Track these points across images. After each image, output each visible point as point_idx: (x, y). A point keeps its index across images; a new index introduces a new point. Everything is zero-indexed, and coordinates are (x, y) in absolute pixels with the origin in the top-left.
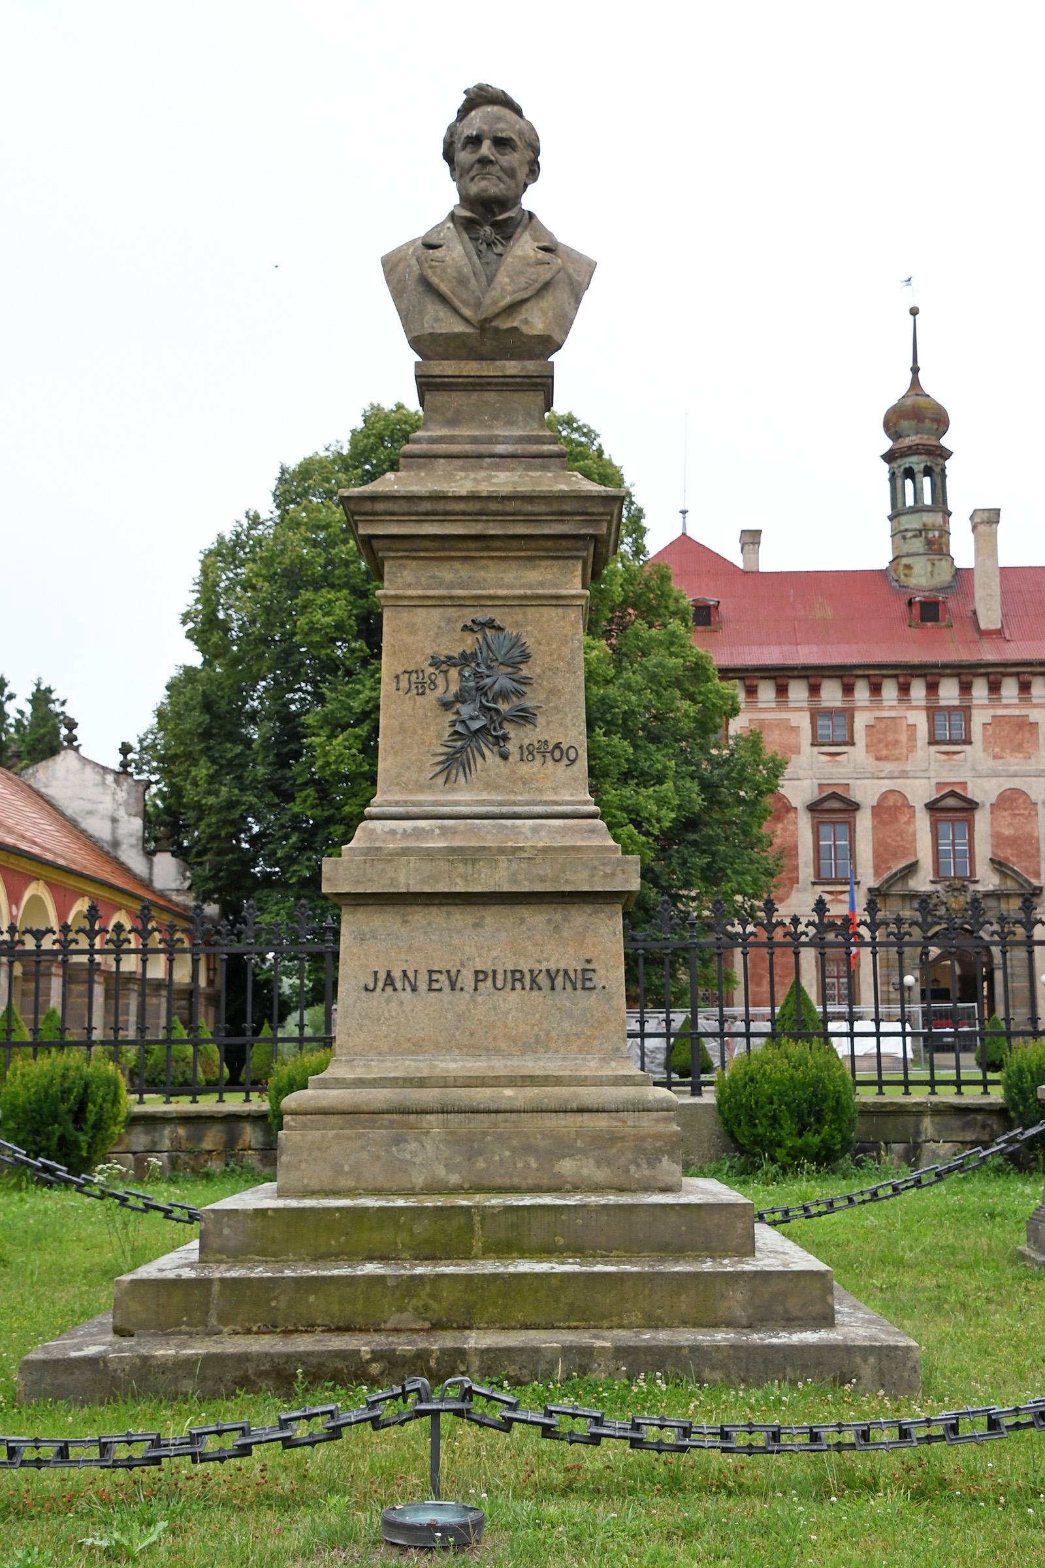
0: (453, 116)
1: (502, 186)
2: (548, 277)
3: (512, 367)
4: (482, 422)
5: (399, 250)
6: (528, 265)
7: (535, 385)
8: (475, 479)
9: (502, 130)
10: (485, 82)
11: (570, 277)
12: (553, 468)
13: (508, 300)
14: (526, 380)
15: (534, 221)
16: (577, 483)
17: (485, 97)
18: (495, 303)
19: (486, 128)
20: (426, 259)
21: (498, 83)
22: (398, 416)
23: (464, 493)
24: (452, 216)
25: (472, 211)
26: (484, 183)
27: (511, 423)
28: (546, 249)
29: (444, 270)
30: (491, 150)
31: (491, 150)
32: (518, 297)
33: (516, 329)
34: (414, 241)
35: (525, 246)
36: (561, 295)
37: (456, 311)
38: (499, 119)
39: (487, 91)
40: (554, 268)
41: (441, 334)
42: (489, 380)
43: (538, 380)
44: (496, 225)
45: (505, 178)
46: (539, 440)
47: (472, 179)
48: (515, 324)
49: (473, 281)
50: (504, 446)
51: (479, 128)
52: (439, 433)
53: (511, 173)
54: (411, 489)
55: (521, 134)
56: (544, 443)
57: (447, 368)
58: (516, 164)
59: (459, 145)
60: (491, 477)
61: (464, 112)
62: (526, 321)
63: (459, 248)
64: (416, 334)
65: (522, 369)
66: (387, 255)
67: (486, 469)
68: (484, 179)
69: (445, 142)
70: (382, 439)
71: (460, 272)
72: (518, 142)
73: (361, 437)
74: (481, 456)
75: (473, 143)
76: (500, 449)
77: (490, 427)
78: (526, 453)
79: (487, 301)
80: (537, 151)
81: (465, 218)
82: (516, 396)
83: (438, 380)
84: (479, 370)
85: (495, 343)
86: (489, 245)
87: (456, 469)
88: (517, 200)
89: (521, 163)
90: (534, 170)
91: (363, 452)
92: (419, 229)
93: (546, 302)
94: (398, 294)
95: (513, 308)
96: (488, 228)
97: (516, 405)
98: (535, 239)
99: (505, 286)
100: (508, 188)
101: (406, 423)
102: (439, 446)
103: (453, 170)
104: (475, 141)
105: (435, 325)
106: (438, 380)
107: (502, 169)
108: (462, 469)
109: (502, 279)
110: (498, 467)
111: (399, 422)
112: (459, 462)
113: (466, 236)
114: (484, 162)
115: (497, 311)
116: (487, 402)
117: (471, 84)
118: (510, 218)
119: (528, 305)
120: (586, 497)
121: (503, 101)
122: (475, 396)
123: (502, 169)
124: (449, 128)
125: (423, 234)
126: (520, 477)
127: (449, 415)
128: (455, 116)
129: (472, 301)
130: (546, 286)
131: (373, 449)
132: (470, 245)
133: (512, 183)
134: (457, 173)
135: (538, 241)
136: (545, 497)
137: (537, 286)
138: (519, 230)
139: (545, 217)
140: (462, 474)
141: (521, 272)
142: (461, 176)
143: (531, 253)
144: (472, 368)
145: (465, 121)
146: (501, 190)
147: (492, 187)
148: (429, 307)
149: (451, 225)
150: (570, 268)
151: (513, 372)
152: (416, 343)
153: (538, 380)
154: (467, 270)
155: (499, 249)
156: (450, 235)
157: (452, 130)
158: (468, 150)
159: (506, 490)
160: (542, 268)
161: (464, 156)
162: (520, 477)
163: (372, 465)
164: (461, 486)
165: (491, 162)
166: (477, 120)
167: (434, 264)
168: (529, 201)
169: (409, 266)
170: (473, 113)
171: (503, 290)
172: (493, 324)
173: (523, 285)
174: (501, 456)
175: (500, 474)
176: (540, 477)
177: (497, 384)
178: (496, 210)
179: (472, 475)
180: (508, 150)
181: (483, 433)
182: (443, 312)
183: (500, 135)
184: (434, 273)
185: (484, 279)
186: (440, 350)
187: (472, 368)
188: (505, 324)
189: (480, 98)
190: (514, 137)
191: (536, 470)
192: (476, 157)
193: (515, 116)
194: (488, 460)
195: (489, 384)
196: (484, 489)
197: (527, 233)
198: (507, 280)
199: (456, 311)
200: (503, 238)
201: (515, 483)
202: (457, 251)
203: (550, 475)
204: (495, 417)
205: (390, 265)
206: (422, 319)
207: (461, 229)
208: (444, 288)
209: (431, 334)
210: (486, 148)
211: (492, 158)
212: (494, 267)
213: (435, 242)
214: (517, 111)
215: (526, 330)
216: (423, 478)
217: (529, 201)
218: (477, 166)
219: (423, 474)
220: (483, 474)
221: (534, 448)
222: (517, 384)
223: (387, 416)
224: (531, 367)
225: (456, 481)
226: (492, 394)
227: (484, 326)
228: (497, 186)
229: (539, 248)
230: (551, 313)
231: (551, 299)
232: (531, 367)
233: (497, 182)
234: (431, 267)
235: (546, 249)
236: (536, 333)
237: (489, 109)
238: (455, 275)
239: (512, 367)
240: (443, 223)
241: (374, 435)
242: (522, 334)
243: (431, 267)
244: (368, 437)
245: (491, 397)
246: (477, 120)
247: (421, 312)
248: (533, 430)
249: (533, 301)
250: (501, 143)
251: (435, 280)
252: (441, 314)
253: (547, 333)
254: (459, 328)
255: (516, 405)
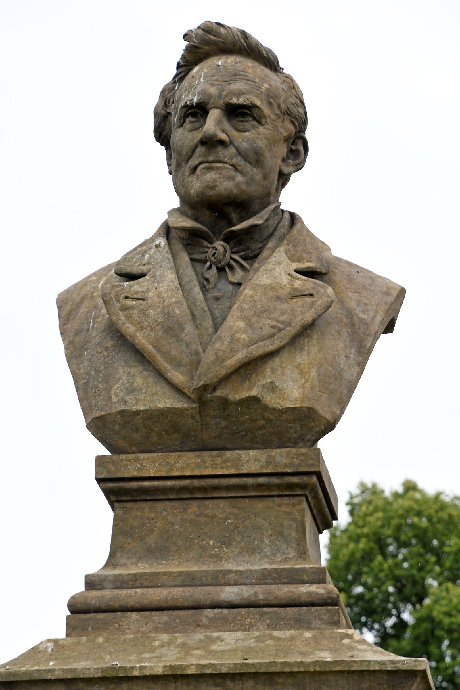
0: (170, 72)
1: (240, 178)
2: (309, 317)
3: (251, 460)
4: (203, 548)
5: (85, 283)
6: (278, 298)
7: (290, 486)
8: (184, 644)
9: (239, 94)
10: (215, 20)
11: (350, 314)
12: (316, 623)
13: (241, 356)
14: (275, 480)
15: (298, 226)
16: (352, 648)
17: (215, 43)
18: (220, 360)
19: (213, 91)
20: (117, 296)
21: (235, 18)
22: (406, 503)
23: (159, 670)
24: (167, 230)
25: (196, 220)
26: (210, 176)
27: (251, 550)
28: (310, 273)
29: (144, 313)
30: (230, 131)
31: (230, 131)
32: (258, 350)
33: (255, 400)
34: (106, 269)
35: (276, 269)
36: (335, 344)
37: (161, 375)
38: (235, 76)
39: (217, 34)
40: (320, 303)
41: (137, 413)
42: (216, 481)
43: (295, 480)
44: (235, 239)
45: (248, 168)
46: (294, 577)
47: (194, 169)
48: (254, 392)
49: (189, 327)
50: (235, 589)
51: (203, 92)
52: (134, 571)
53: (255, 158)
54: (75, 666)
55: (271, 97)
56: (303, 582)
57: (150, 465)
58: (262, 144)
59: (175, 119)
60: (212, 640)
61: (185, 67)
62: (272, 388)
63: (171, 276)
64: (98, 414)
65: (268, 463)
66: (68, 291)
67: (207, 627)
68: (209, 169)
69: (156, 114)
70: (382, 547)
71: (168, 315)
72: (266, 110)
73: (345, 540)
74: (198, 607)
75: (194, 115)
76: (230, 593)
77: (218, 558)
78: (272, 600)
79: (208, 357)
80: (301, 122)
81: (183, 229)
82: (260, 505)
83: (134, 485)
84: (198, 466)
85: (224, 423)
86: (221, 270)
87: (157, 630)
88: (268, 197)
89: (272, 143)
90: (297, 150)
91: (348, 566)
92: (112, 252)
93: (308, 356)
94: (74, 354)
95: (251, 366)
96: (219, 244)
97: (260, 521)
98: (293, 258)
99: (239, 332)
100: (251, 181)
101: (419, 514)
102: (131, 592)
103: (169, 157)
104: (198, 111)
105: (130, 399)
106: (134, 485)
107: (239, 153)
108: (168, 628)
109: (235, 322)
110: (224, 625)
111: (408, 511)
112: (163, 617)
113: (184, 258)
114: (210, 143)
115: (223, 372)
116: (214, 516)
117: (193, 24)
118: (254, 227)
119: (277, 361)
120: (361, 673)
121: (245, 47)
122: (194, 507)
123: (239, 153)
124: (163, 92)
125: (117, 257)
126: (258, 639)
127: (152, 540)
128: (174, 71)
129: (186, 360)
130: (307, 329)
131: (367, 557)
132: (189, 272)
133: (257, 174)
134: (174, 161)
135: (299, 260)
136: (291, 674)
137: (291, 331)
138: (270, 244)
139: (314, 223)
140: (165, 637)
141: (265, 311)
142: (179, 165)
143: (285, 280)
144: (187, 463)
145: (185, 83)
146: (237, 185)
147: (222, 180)
148: (121, 371)
149: (162, 241)
150: (352, 300)
151: (254, 468)
152: (98, 426)
153: (295, 480)
154: (180, 311)
155: (238, 275)
156: (158, 256)
157: (167, 96)
158: (188, 125)
159: (227, 663)
160: (300, 302)
161: (183, 136)
162: (258, 639)
163: (365, 585)
164: (159, 658)
165: (222, 143)
166: (203, 81)
167: (129, 303)
168: (289, 199)
169: (95, 308)
170: (196, 69)
171: (234, 340)
172: (218, 393)
173: (267, 330)
174: (232, 606)
175: (225, 635)
176: (292, 638)
177: (229, 488)
178: (234, 216)
179: (180, 639)
180: (250, 123)
181: (204, 568)
182: (140, 378)
183: (234, 100)
184: (129, 318)
185: (208, 323)
186: (137, 436)
187: (187, 463)
188: (237, 393)
189: (208, 44)
190: (258, 103)
191: (288, 627)
192: (198, 136)
193: (261, 70)
194: (210, 613)
195: (216, 488)
196: (195, 661)
197: (282, 248)
198: (241, 324)
199: (161, 375)
200: (245, 259)
201: (249, 650)
202: (167, 284)
203: (308, 634)
204: (226, 542)
205: (68, 308)
206: (109, 391)
207: (178, 246)
208: (142, 340)
209: (122, 412)
210: (213, 123)
211: (223, 136)
212: (228, 304)
213: (135, 269)
214: (270, 62)
215: (271, 400)
216: (100, 646)
217: (289, 199)
218: (200, 150)
219: (101, 640)
220: (199, 636)
221: (285, 591)
222: (259, 486)
223: (387, 503)
224: (282, 458)
225: (153, 650)
226: (222, 503)
227: (203, 396)
228: (232, 178)
229: (296, 271)
230: (313, 373)
231: (314, 350)
232: (282, 458)
233: (232, 173)
234: (124, 308)
235: (310, 273)
236: (289, 405)
237: (220, 61)
238: (160, 319)
239: (251, 460)
240: (153, 239)
241: (366, 536)
242: (266, 408)
243: (124, 308)
244: (357, 539)
245: (220, 508)
246: (203, 81)
247: (108, 380)
248: (286, 560)
249: (285, 355)
250: (236, 112)
251: (129, 329)
252: (139, 381)
253: (306, 404)
254: (166, 401)
255: (260, 521)
